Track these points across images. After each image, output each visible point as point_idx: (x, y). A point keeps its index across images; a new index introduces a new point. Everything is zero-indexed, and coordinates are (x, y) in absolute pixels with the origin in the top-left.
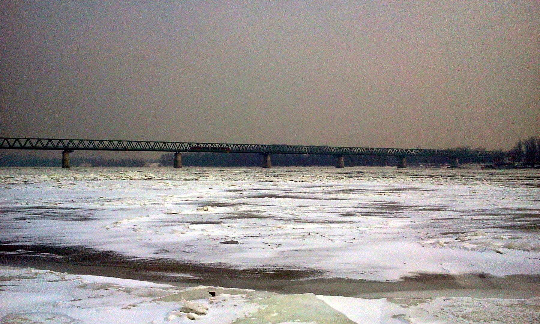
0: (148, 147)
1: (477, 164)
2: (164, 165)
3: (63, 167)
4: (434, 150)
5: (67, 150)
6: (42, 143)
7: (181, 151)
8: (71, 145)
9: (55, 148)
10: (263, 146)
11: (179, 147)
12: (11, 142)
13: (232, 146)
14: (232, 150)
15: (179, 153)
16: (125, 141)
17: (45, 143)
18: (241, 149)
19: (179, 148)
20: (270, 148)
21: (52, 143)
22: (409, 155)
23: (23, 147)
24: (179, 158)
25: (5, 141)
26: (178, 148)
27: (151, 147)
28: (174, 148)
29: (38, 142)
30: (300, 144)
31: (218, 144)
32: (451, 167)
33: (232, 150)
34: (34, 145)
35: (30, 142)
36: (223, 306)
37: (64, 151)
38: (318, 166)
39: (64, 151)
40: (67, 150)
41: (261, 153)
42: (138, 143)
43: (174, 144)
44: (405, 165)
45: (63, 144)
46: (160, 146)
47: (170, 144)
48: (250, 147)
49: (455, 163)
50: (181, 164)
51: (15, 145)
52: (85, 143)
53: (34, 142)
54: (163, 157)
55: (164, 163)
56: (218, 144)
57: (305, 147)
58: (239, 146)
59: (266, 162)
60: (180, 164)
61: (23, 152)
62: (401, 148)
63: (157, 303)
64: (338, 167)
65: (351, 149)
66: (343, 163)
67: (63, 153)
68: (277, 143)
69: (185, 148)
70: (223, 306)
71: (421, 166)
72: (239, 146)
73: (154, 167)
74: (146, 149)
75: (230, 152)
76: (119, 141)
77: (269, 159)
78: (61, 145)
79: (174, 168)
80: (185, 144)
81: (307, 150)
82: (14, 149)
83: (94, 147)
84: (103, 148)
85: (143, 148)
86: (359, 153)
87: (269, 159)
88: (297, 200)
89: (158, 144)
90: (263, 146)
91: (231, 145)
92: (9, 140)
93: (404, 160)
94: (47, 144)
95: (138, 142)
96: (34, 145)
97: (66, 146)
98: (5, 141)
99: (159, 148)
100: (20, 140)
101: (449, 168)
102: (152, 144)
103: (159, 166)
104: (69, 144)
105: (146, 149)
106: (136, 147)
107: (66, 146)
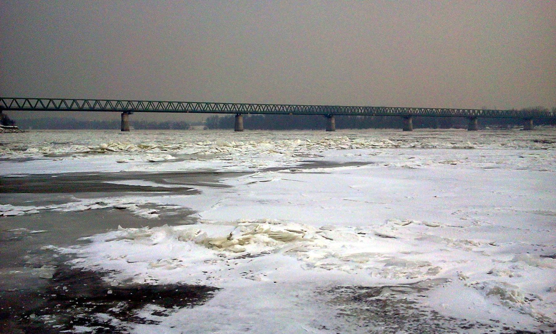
0: (217, 109)
1: (550, 126)
2: (210, 128)
3: (122, 130)
4: (498, 111)
5: (126, 112)
6: (77, 104)
7: (242, 113)
8: (130, 107)
9: (114, 110)
10: (320, 107)
11: (240, 108)
12: (33, 103)
13: (279, 107)
14: (279, 111)
15: (240, 115)
16: (203, 103)
17: (69, 103)
18: (273, 110)
19: (223, 109)
20: (320, 109)
21: (88, 104)
22: (417, 115)
23: (81, 109)
24: (241, 120)
25: (27, 102)
26: (230, 109)
27: (183, 108)
28: (217, 109)
29: (61, 102)
30: (355, 105)
31: (231, 104)
32: (524, 130)
33: (279, 111)
34: (58, 106)
35: (54, 103)
36: (490, 273)
37: (123, 113)
38: (375, 129)
39: (123, 113)
40: (126, 112)
41: (326, 116)
42: (188, 105)
43: (234, 106)
44: (477, 127)
45: (100, 105)
46: (212, 108)
47: (222, 105)
48: (298, 108)
49: (529, 124)
50: (243, 127)
51: (25, 105)
52: (134, 104)
53: (57, 103)
54: (208, 119)
55: (211, 126)
56: (302, 106)
57: (361, 108)
58: (295, 107)
59: (408, 124)
60: (242, 126)
61: (59, 114)
62: (463, 108)
63: (342, 287)
64: (405, 130)
65: (384, 110)
66: (412, 125)
67: (122, 115)
68: (313, 104)
69: (229, 110)
70: (490, 273)
71: (488, 128)
72: (295, 107)
73: (199, 130)
74: (197, 110)
75: (293, 114)
76: (150, 102)
77: (333, 121)
78: (119, 107)
79: (327, 131)
80: (220, 104)
81: (360, 111)
82: (11, 110)
83: (153, 108)
84: (142, 110)
85: (185, 109)
86: (417, 114)
87: (333, 121)
88: (312, 172)
89: (191, 105)
90: (259, 105)
91: (263, 106)
92: (42, 101)
93: (476, 122)
94: (83, 105)
95: (170, 102)
96: (58, 106)
97: (92, 107)
98: (14, 101)
99: (193, 109)
100: (54, 100)
101: (522, 130)
102: (176, 104)
103: (205, 129)
104: (106, 105)
105: (178, 110)
106: (177, 108)
107: (92, 107)
